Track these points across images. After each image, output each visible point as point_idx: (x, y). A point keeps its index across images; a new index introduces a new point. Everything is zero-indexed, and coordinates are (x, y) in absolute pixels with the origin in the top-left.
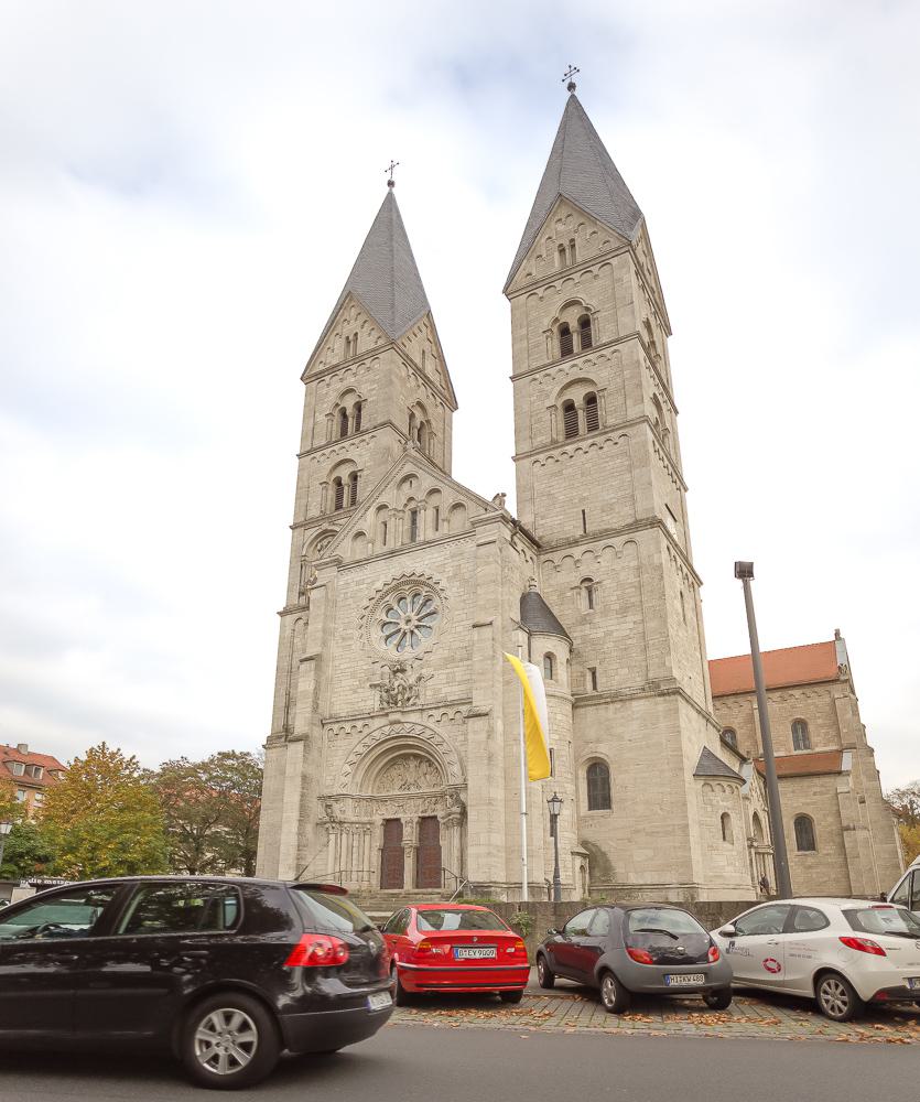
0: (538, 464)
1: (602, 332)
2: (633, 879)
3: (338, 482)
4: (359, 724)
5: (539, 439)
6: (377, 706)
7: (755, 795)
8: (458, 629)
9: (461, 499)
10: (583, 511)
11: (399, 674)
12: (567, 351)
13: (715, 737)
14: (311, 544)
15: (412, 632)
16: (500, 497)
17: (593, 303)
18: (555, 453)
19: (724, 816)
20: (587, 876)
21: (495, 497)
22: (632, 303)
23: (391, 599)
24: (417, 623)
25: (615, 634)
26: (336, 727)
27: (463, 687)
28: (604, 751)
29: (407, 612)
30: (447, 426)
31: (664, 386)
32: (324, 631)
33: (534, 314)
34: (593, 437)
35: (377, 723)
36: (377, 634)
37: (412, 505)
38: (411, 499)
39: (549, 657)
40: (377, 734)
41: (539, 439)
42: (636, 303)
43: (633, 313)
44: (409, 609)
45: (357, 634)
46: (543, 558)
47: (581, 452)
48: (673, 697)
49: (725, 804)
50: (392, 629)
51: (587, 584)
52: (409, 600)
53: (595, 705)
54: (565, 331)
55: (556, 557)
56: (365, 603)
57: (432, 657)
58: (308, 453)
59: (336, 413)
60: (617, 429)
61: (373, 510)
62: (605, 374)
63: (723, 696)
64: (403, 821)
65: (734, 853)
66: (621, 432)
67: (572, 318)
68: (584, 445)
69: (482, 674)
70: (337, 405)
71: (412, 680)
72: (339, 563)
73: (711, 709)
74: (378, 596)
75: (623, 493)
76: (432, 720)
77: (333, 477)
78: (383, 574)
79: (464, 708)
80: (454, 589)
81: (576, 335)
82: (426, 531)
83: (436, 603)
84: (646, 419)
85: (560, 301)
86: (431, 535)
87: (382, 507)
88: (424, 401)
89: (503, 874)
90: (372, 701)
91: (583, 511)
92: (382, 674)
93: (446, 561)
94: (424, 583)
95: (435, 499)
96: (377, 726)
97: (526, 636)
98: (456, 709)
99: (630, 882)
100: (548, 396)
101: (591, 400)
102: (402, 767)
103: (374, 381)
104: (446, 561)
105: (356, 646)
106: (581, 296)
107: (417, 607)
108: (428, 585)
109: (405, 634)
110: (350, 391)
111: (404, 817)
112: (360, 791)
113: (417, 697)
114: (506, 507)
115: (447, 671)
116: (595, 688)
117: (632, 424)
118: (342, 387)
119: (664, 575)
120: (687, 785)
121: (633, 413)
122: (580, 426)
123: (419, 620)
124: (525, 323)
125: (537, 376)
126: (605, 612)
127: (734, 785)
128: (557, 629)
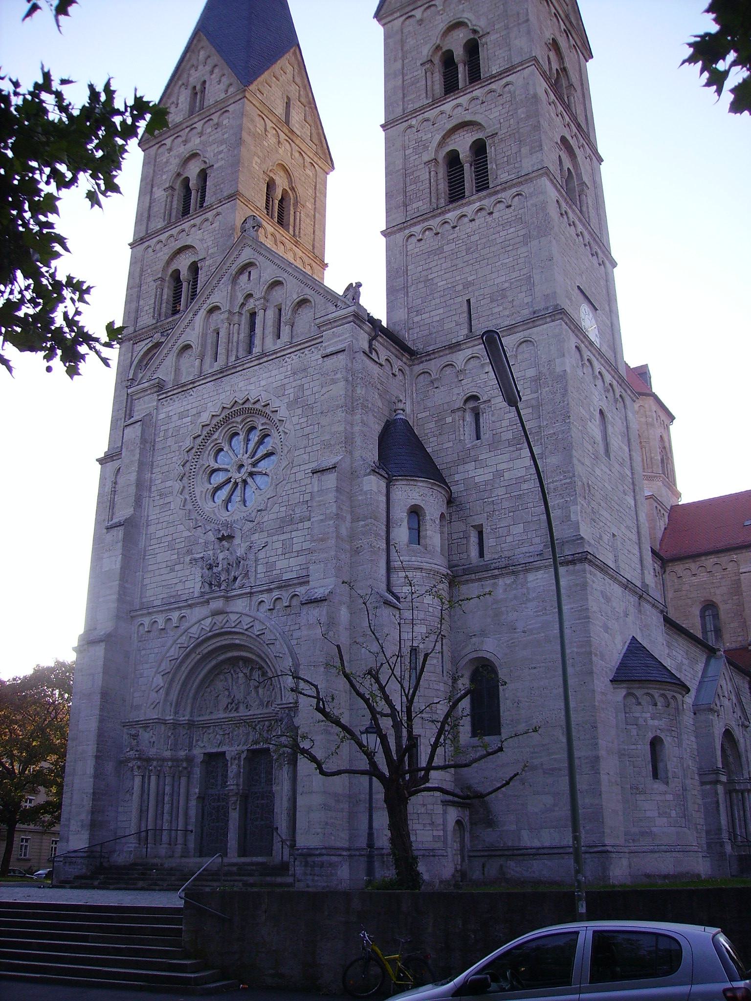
0: (413, 240)
1: (492, 60)
2: (528, 840)
3: (176, 274)
4: (175, 616)
5: (415, 206)
7: (726, 702)
8: (300, 476)
9: (308, 293)
10: (468, 301)
11: (224, 543)
12: (451, 87)
13: (655, 619)
14: (140, 361)
16: (354, 290)
17: (481, 24)
18: (434, 223)
19: (656, 744)
20: (467, 835)
21: (348, 289)
22: (528, 20)
24: (250, 469)
25: (507, 475)
27: (301, 560)
28: (490, 647)
29: (237, 452)
30: (596, 176)
31: (579, 126)
33: (411, 42)
34: (480, 199)
38: (250, 296)
39: (415, 512)
41: (415, 206)
42: (532, 18)
43: (529, 32)
45: (178, 486)
46: (418, 369)
47: (466, 220)
48: (578, 567)
49: (656, 722)
51: (471, 404)
52: (241, 437)
53: (480, 580)
54: (448, 61)
55: (433, 366)
56: (188, 443)
57: (266, 517)
59: (178, 186)
60: (510, 188)
62: (495, 114)
63: (700, 555)
64: (228, 757)
65: (669, 797)
66: (514, 191)
67: (457, 43)
68: (469, 210)
69: (322, 540)
71: (240, 552)
73: (650, 579)
74: (205, 433)
77: (170, 271)
78: (210, 401)
79: (301, 590)
80: (295, 420)
81: (461, 68)
82: (265, 341)
84: (545, 171)
85: (441, 23)
86: (270, 345)
88: (288, 162)
89: (344, 835)
90: (192, 582)
93: (286, 381)
94: (260, 413)
97: (383, 484)
99: (523, 844)
100: (426, 148)
101: (479, 149)
102: (229, 676)
103: (222, 142)
104: (286, 381)
105: (176, 502)
106: (467, 16)
107: (251, 445)
108: (266, 416)
110: (194, 155)
111: (230, 750)
112: (176, 713)
113: (246, 575)
114: (362, 302)
116: (481, 554)
117: (526, 179)
118: (183, 150)
119: (570, 389)
120: (598, 697)
121: (528, 164)
122: (467, 185)
123: (254, 465)
124: (400, 55)
125: (413, 122)
126: (494, 445)
127: (669, 694)
128: (427, 468)
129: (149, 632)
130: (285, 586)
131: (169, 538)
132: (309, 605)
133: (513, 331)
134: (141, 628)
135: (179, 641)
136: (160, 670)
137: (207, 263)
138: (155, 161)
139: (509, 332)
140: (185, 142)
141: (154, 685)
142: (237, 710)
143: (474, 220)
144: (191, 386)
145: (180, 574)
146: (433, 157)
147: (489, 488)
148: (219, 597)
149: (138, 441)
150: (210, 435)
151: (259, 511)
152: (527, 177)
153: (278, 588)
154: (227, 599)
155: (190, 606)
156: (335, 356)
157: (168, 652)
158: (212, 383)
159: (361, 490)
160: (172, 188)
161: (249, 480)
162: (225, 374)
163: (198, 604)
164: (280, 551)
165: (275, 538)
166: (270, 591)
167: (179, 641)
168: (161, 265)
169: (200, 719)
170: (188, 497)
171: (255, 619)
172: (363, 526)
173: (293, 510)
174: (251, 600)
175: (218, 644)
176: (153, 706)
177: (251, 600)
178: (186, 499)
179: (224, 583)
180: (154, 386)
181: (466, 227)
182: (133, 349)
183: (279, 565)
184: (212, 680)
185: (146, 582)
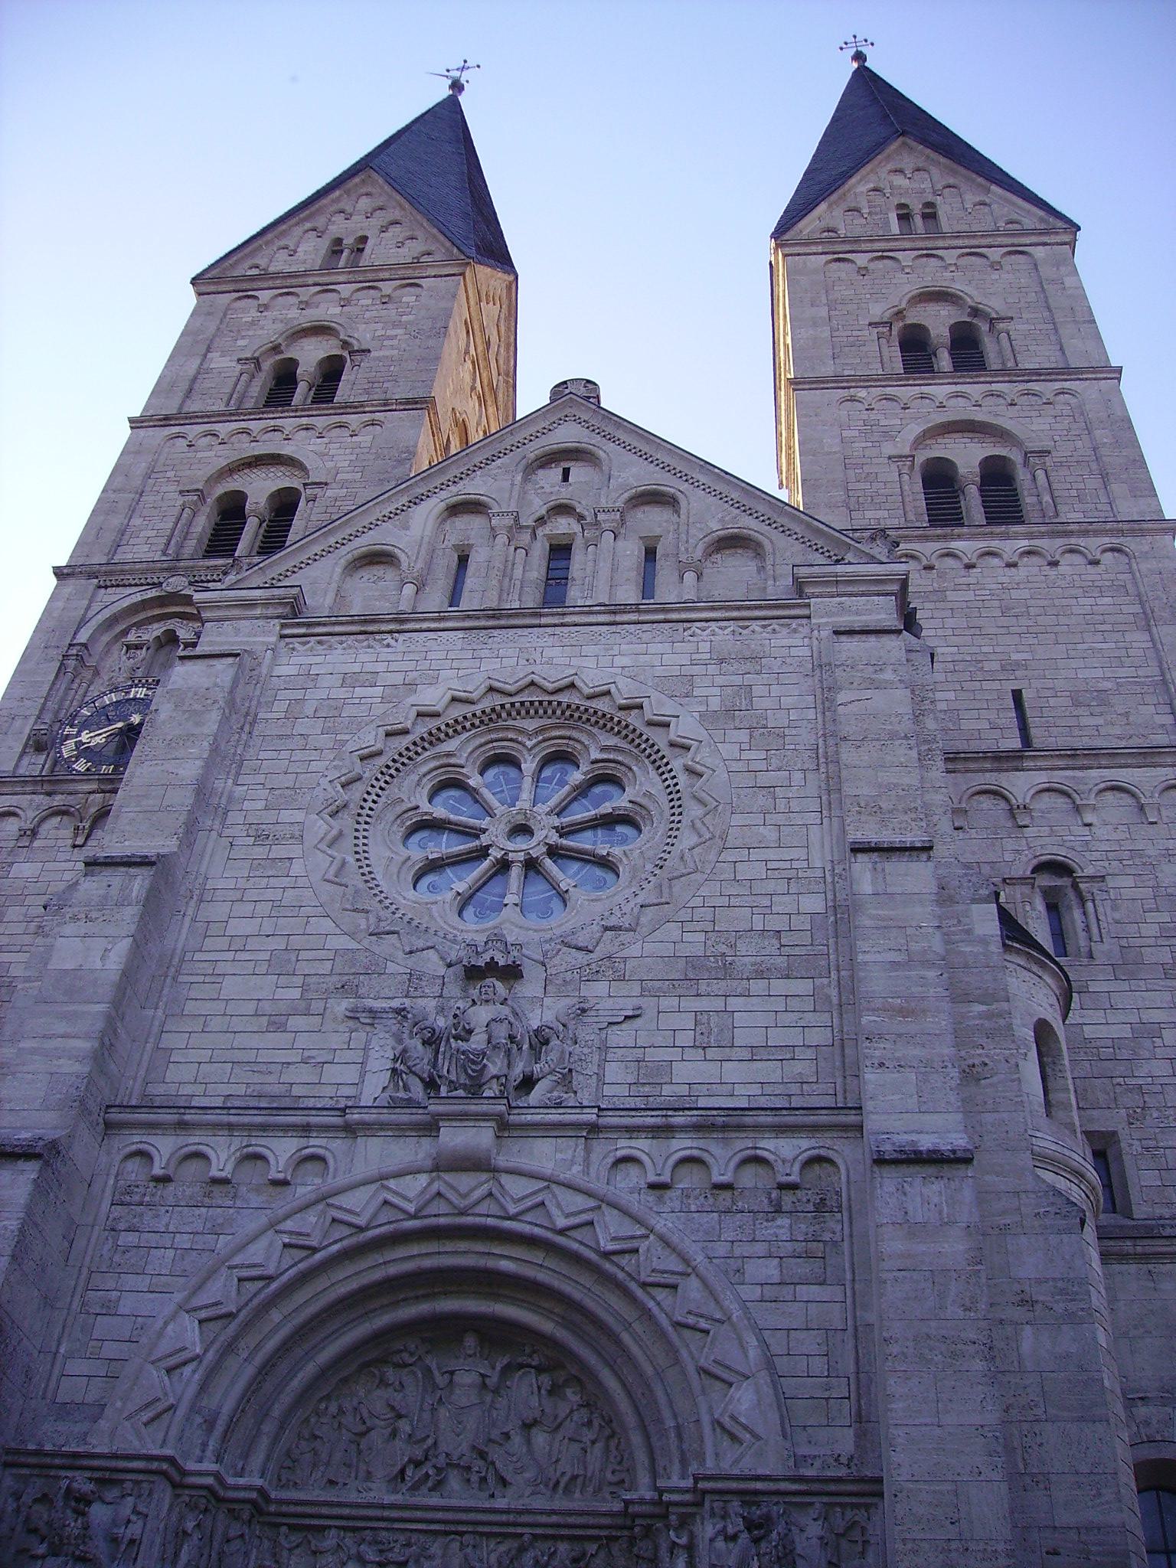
4: (282, 1150)
6: (375, 1086)
8: (745, 871)
10: (1017, 695)
15: (483, 852)
23: (462, 749)
24: (554, 838)
26: (164, 1147)
29: (526, 803)
32: (202, 791)
35: (376, 1153)
36: (390, 854)
37: (563, 525)
40: (360, 1204)
41: (869, 514)
44: (526, 795)
47: (995, 561)
50: (446, 845)
56: (371, 738)
58: (166, 421)
61: (434, 506)
70: (276, 349)
72: (293, 610)
75: (1132, 672)
76: (631, 1177)
77: (220, 490)
78: (452, 669)
83: (643, 785)
87: (472, 507)
91: (1017, 695)
92: (413, 977)
93: (696, 670)
94: (604, 722)
95: (653, 519)
96: (361, 1171)
98: (742, 1144)
105: (310, 865)
109: (504, 866)
113: (566, 1080)
115: (702, 1004)
129: (165, 1180)
130: (725, 1127)
131: (279, 944)
132: (904, 1169)
133: (1149, 760)
134: (133, 1165)
135: (289, 1225)
136: (197, 1302)
137: (329, 493)
138: (225, 315)
139: (1140, 760)
140: (304, 305)
141: (165, 1346)
142: (438, 1486)
143: (1015, 565)
144: (392, 627)
145: (302, 1041)
146: (907, 451)
147: (1125, 1054)
148: (485, 1117)
149: (221, 696)
150: (433, 739)
151: (606, 929)
152: (1136, 526)
153: (697, 1128)
154: (504, 1127)
155: (350, 1130)
156: (872, 638)
157: (242, 1247)
158: (460, 634)
159: (968, 932)
160: (257, 362)
161: (516, 872)
162: (502, 622)
163: (383, 1126)
164: (685, 1038)
165: (667, 1003)
166: (663, 1131)
167: (289, 1225)
168: (210, 470)
169: (286, 1495)
170: (351, 859)
171: (604, 1201)
172: (980, 1016)
173: (733, 946)
174: (588, 1151)
175: (428, 1263)
176: (146, 1416)
177: (588, 1151)
178: (344, 863)
179: (494, 1084)
180: (281, 602)
181: (992, 573)
182: (94, 595)
183: (684, 1072)
184: (345, 1380)
185: (168, 1041)
